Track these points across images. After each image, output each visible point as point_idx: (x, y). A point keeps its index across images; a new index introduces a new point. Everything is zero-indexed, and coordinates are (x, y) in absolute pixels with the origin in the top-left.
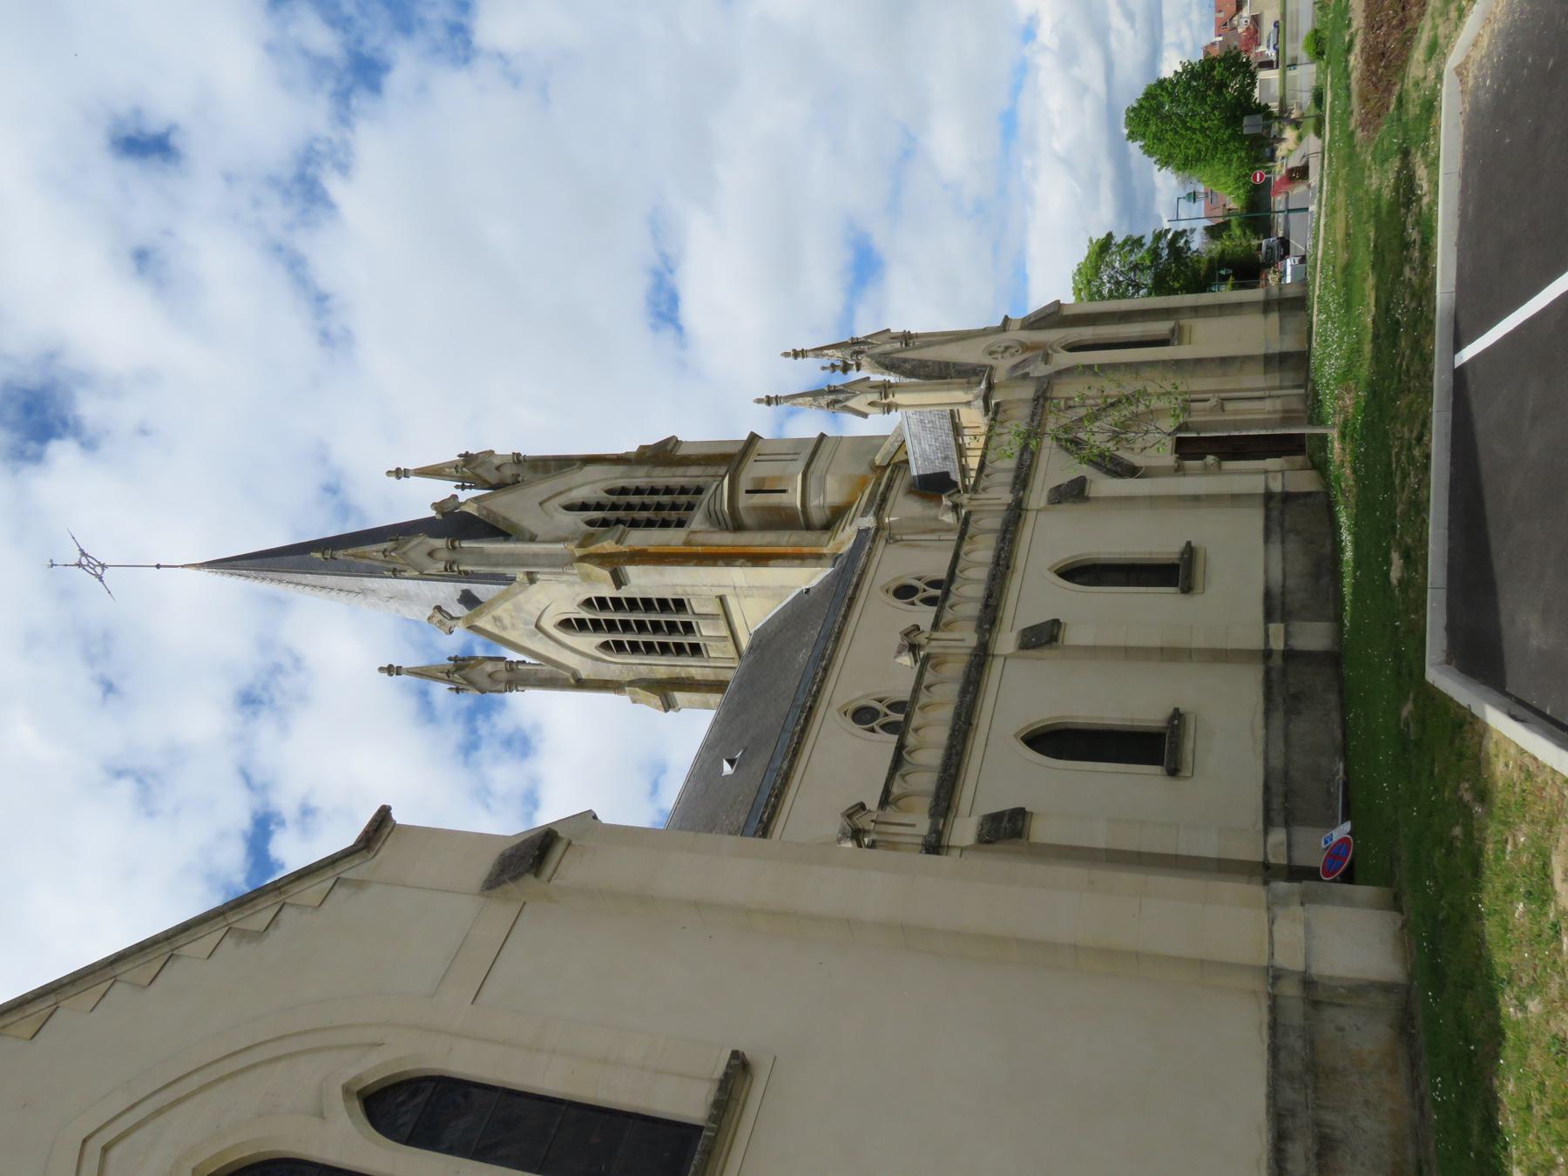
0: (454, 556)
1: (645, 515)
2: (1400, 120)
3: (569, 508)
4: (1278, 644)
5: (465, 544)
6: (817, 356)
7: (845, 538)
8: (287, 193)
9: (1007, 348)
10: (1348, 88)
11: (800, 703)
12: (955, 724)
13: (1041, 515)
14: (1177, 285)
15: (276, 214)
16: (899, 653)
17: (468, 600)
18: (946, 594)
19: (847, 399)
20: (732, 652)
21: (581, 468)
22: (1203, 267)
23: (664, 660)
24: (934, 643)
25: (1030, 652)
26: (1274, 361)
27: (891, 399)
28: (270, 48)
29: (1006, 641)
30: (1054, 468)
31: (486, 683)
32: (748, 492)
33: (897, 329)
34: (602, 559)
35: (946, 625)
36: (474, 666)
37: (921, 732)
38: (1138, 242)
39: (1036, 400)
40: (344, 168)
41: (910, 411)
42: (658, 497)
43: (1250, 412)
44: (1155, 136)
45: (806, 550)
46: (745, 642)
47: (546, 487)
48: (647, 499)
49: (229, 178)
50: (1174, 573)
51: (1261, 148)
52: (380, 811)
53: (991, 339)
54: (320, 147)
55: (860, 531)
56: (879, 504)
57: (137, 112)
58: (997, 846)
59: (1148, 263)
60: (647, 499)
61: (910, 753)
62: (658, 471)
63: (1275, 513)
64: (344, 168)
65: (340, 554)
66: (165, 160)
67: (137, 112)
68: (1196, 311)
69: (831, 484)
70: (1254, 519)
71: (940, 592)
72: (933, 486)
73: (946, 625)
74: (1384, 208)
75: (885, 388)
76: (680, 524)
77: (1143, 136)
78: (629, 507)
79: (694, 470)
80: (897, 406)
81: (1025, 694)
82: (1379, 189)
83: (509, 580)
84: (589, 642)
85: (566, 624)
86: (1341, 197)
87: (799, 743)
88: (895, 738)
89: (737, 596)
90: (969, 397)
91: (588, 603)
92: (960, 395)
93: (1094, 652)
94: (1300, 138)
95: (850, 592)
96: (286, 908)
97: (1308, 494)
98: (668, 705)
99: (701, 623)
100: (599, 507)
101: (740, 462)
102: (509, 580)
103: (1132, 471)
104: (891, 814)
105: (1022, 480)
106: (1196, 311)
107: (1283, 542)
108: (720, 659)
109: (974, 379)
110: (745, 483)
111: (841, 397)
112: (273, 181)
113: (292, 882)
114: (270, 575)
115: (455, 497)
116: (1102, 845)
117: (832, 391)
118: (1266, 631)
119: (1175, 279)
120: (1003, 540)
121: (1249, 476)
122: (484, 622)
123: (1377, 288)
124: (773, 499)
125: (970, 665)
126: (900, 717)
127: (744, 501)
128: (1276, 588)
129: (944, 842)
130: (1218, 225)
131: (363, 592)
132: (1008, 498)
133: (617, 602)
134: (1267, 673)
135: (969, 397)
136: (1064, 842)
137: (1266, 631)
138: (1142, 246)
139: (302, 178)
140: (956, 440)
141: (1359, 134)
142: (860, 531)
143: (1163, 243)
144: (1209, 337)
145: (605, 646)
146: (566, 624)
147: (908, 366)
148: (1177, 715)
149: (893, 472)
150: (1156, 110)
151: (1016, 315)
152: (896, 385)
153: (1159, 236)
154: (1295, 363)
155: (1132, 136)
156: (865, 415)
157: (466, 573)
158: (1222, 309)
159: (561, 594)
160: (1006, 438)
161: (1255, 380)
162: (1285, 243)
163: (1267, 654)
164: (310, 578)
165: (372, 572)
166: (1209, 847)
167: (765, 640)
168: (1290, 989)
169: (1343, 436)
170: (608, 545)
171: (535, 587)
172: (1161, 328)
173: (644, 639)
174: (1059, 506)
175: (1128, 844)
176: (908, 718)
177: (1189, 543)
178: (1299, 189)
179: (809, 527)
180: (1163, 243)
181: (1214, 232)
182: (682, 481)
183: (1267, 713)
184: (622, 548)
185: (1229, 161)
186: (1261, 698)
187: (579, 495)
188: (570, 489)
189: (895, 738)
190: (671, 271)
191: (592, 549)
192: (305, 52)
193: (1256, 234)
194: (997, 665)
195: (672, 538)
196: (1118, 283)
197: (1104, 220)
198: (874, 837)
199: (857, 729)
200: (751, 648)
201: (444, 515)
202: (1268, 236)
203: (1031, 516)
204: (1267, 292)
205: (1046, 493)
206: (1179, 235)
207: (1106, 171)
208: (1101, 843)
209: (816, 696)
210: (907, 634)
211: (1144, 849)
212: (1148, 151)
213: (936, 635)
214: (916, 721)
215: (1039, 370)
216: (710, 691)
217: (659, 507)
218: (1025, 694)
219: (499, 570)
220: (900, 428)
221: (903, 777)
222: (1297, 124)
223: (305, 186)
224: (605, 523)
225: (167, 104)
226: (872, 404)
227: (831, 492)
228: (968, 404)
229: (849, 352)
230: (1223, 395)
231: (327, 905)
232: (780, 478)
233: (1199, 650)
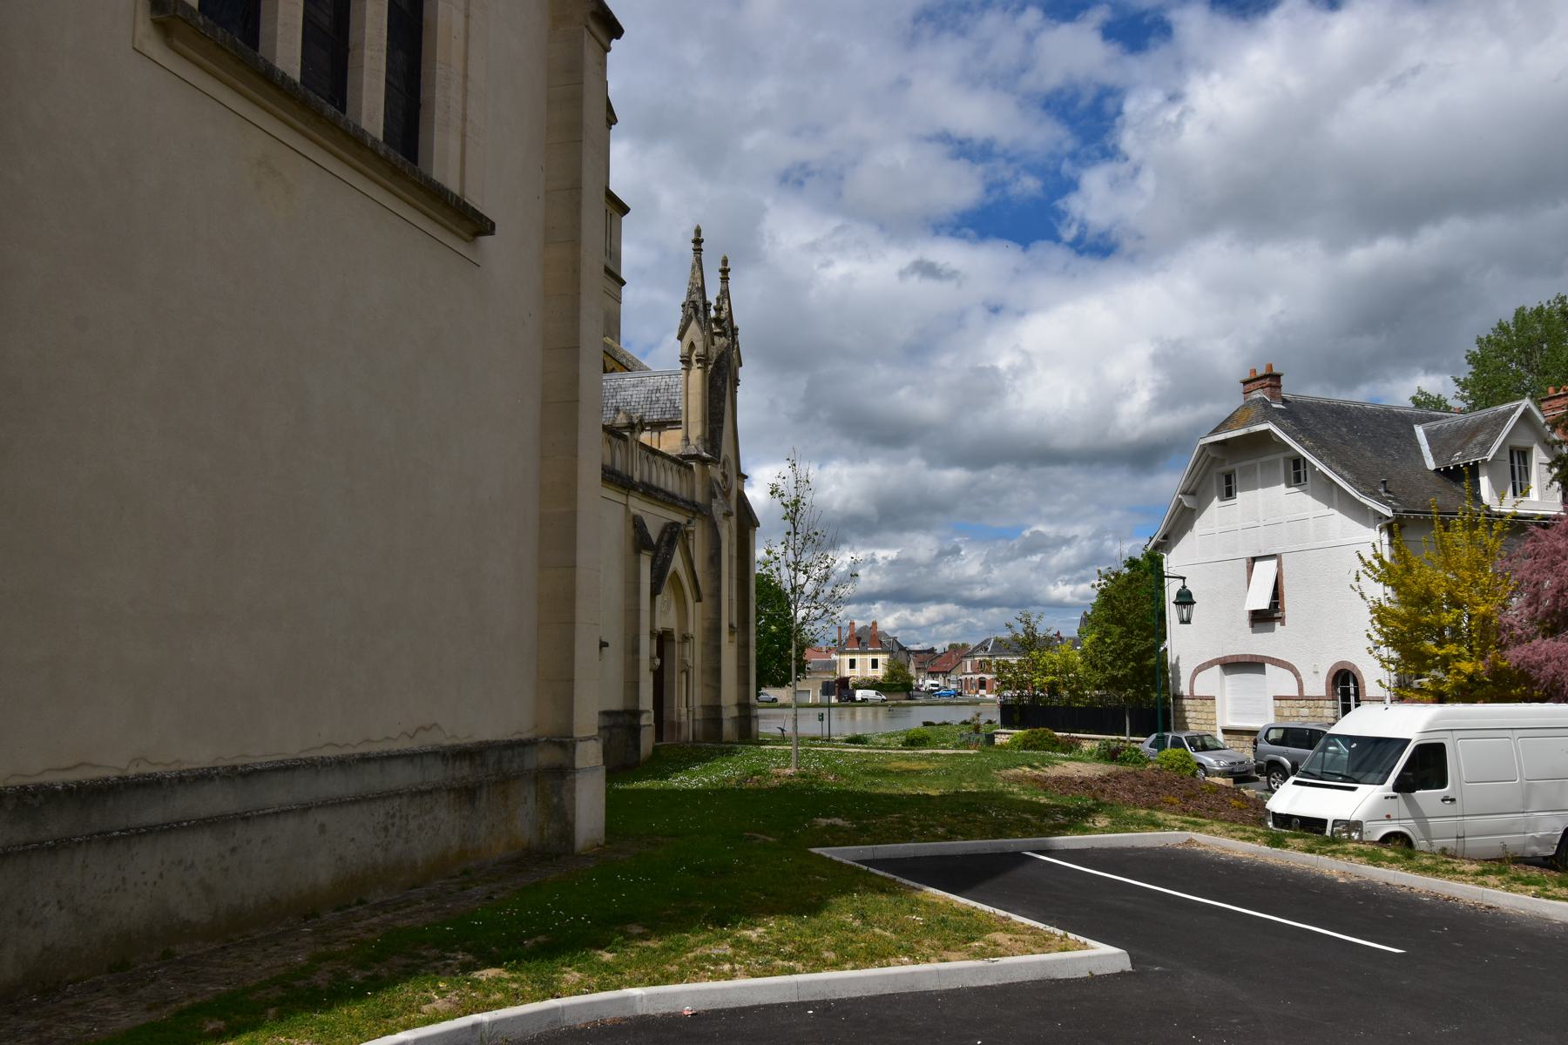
13: (622, 508)
19: (699, 322)
27: (695, 365)
30: (656, 518)
39: (693, 504)
63: (621, 720)
80: (688, 370)
92: (696, 431)
103: (655, 591)
111: (701, 316)
135: (693, 440)
156: (680, 337)
161: (698, 697)
168: (546, 757)
174: (630, 525)
215: (717, 508)
226: (692, 346)
228: (687, 439)
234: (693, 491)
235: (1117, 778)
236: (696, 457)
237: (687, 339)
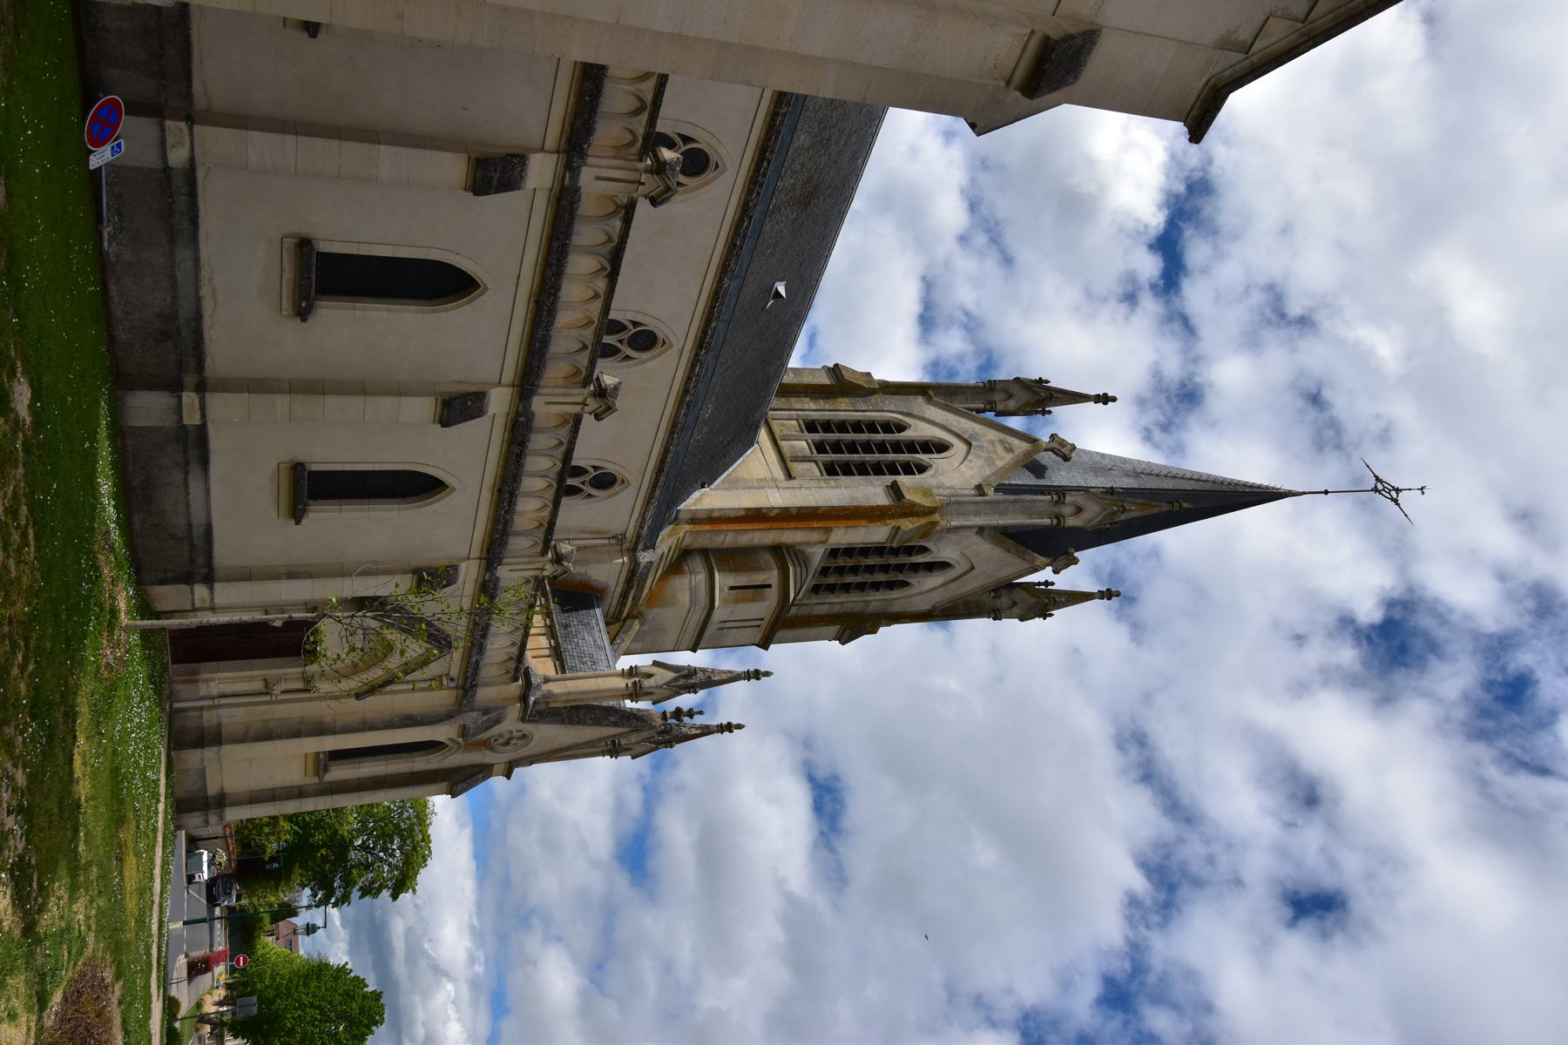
0: (1056, 509)
1: (870, 561)
2: (42, 976)
3: (944, 565)
4: (190, 398)
5: (1047, 521)
6: (707, 727)
7: (667, 541)
8: (1185, 873)
9: (507, 743)
10: (127, 1033)
11: (711, 354)
12: (554, 303)
13: (537, 142)
14: (323, 851)
15: (1193, 852)
16: (616, 388)
17: (1038, 470)
18: (561, 477)
19: (675, 679)
20: (775, 425)
21: (934, 608)
22: (298, 871)
23: (843, 415)
24: (579, 399)
25: (472, 389)
26: (213, 738)
27: (630, 682)
28: (1208, 1008)
29: (499, 402)
30: (451, 606)
31: (1015, 389)
32: (770, 586)
33: (625, 760)
34: (912, 511)
35: (566, 422)
36: (1026, 404)
37: (590, 293)
38: (365, 892)
40: (1133, 902)
41: (607, 671)
42: (856, 586)
43: (234, 680)
44: (353, 998)
45: (708, 527)
46: (763, 434)
47: (971, 584)
48: (868, 578)
49: (1238, 882)
50: (312, 488)
51: (237, 990)
52: (1202, 136)
53: (523, 752)
54: (1155, 919)
55: (653, 547)
56: (634, 576)
57: (1325, 936)
58: (504, 151)
59: (355, 872)
60: (868, 578)
61: (603, 268)
62: (858, 608)
63: (201, 560)
64: (1133, 902)
65: (1165, 507)
66: (1296, 893)
67: (1325, 936)
68: (300, 793)
69: (685, 598)
70: (224, 553)
71: (571, 480)
72: (574, 596)
73: (566, 422)
74: (62, 870)
75: (635, 694)
76: (834, 553)
77: (365, 996)
78: (885, 569)
79: (822, 610)
81: (474, 340)
82: (72, 899)
83: (1000, 488)
84: (918, 431)
85: (942, 447)
86: (132, 904)
87: (712, 308)
88: (613, 315)
89: (774, 480)
90: (545, 687)
91: (922, 469)
92: (556, 688)
93: (399, 390)
94: (199, 1005)
95: (662, 478)
96: (1302, 17)
97: (163, 582)
98: (836, 370)
99: (808, 453)
100: (916, 568)
101: (778, 617)
102: (1000, 488)
103: (360, 603)
104: (621, 192)
105: (488, 588)
106: (300, 793)
107: (190, 525)
108: (786, 418)
109: (542, 707)
110: (772, 595)
111: (682, 682)
112: (1198, 883)
113: (1297, 47)
114: (1224, 488)
115: (1056, 572)
116: (382, 147)
117: (692, 689)
118: (203, 415)
119: (325, 859)
120: (506, 523)
121: (231, 603)
122: (1021, 446)
123: (70, 780)
124: (742, 580)
125: (538, 376)
126: (607, 339)
127: (772, 577)
128: (195, 469)
129: (563, 157)
130: (283, 918)
131: (1136, 474)
132: (502, 572)
133: (892, 469)
134: (200, 367)
135: (545, 687)
136: (429, 153)
137: (203, 415)
138: (361, 889)
139: (1171, 888)
140: (557, 643)
141: (108, 975)
142: (653, 547)
143: (338, 893)
144: (284, 763)
145: (901, 428)
146: (942, 447)
147: (612, 719)
148: (303, 313)
149: (621, 613)
150: (352, 1023)
151: (497, 782)
152: (624, 697)
153: (344, 900)
154: (185, 736)
155: (377, 996)
157: (1043, 493)
158: (272, 796)
159: (954, 474)
160: (507, 629)
161: (233, 717)
162: (212, 901)
163: (201, 388)
164: (1187, 486)
165: (1130, 492)
166: (260, 146)
167: (745, 439)
169: (114, 612)
170: (907, 525)
171: (976, 482)
172: (339, 773)
173: (861, 430)
175: (354, 151)
176: (598, 340)
177: (298, 522)
178: (198, 953)
179: (705, 553)
180: (338, 893)
181: (289, 911)
182: (833, 599)
183: (198, 317)
184: (893, 523)
185: (273, 977)
186: (206, 335)
187: (935, 580)
188: (943, 585)
189: (613, 315)
190: (822, 833)
191: (923, 521)
192: (1176, 1007)
193: (243, 909)
194: (509, 375)
195: (843, 536)
196: (384, 850)
197: (400, 914)
198: (641, 165)
199: (652, 325)
200: (754, 430)
201: (1067, 553)
202: (230, 909)
203: (476, 553)
204: (221, 818)
205: (461, 579)
206: (324, 902)
207: (399, 967)
208: (385, 151)
209: (695, 361)
210: (610, 409)
211: (335, 143)
212: (360, 982)
213: (577, 409)
214: (589, 334)
215: (471, 718)
216: (795, 386)
217: (855, 570)
218: (474, 340)
219: (1012, 497)
220: (616, 658)
221: (610, 240)
222: (203, 1019)
223: (1169, 883)
224: (910, 550)
225: (1296, 948)
226: (650, 676)
227: (687, 587)
228: (547, 680)
229: (674, 733)
230: (267, 698)
231: (1263, 18)
232: (736, 601)
233: (280, 391)
234: (488, 684)
235: (26, 363)
236: (528, 684)
237: (655, 670)
